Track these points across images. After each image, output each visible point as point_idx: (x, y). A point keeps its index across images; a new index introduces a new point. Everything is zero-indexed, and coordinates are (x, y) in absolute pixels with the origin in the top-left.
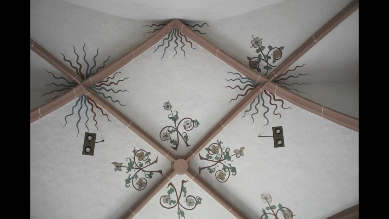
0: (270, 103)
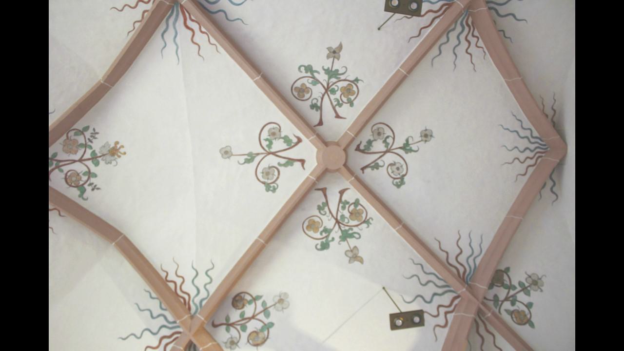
0: (440, 306)
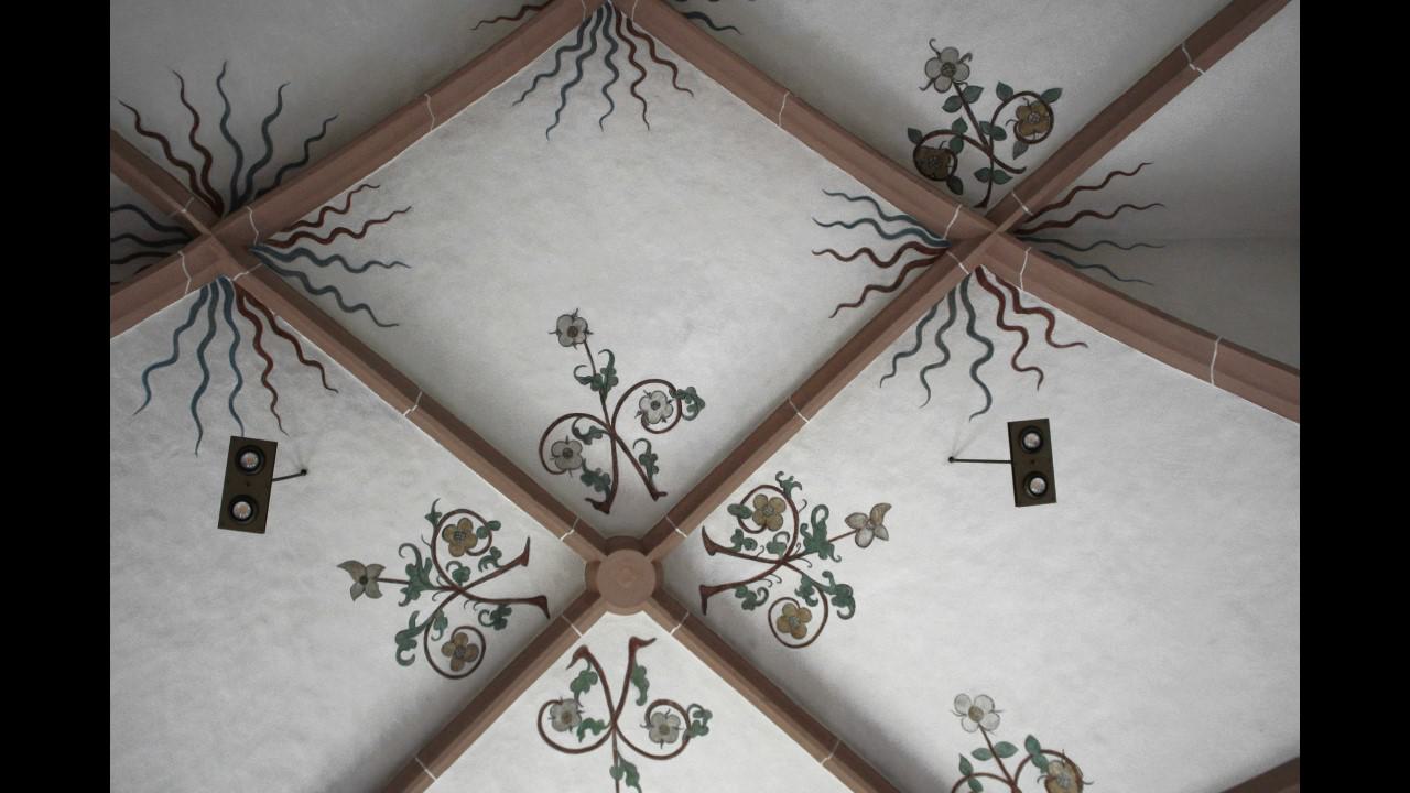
0: (1000, 323)
